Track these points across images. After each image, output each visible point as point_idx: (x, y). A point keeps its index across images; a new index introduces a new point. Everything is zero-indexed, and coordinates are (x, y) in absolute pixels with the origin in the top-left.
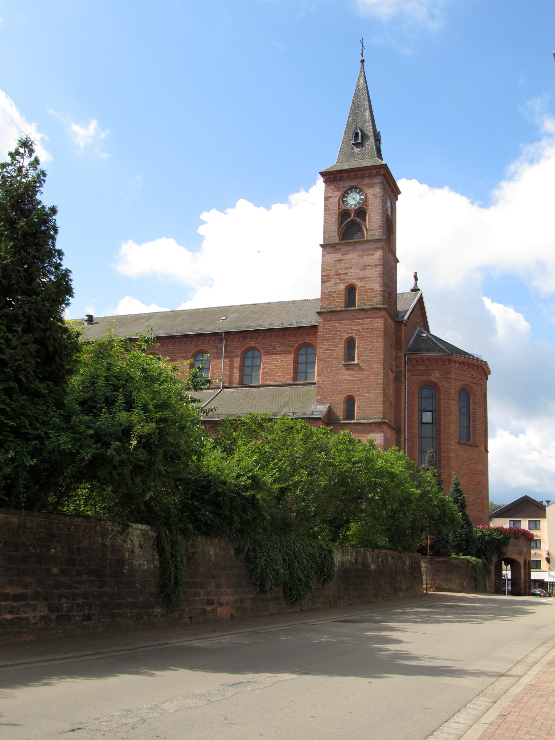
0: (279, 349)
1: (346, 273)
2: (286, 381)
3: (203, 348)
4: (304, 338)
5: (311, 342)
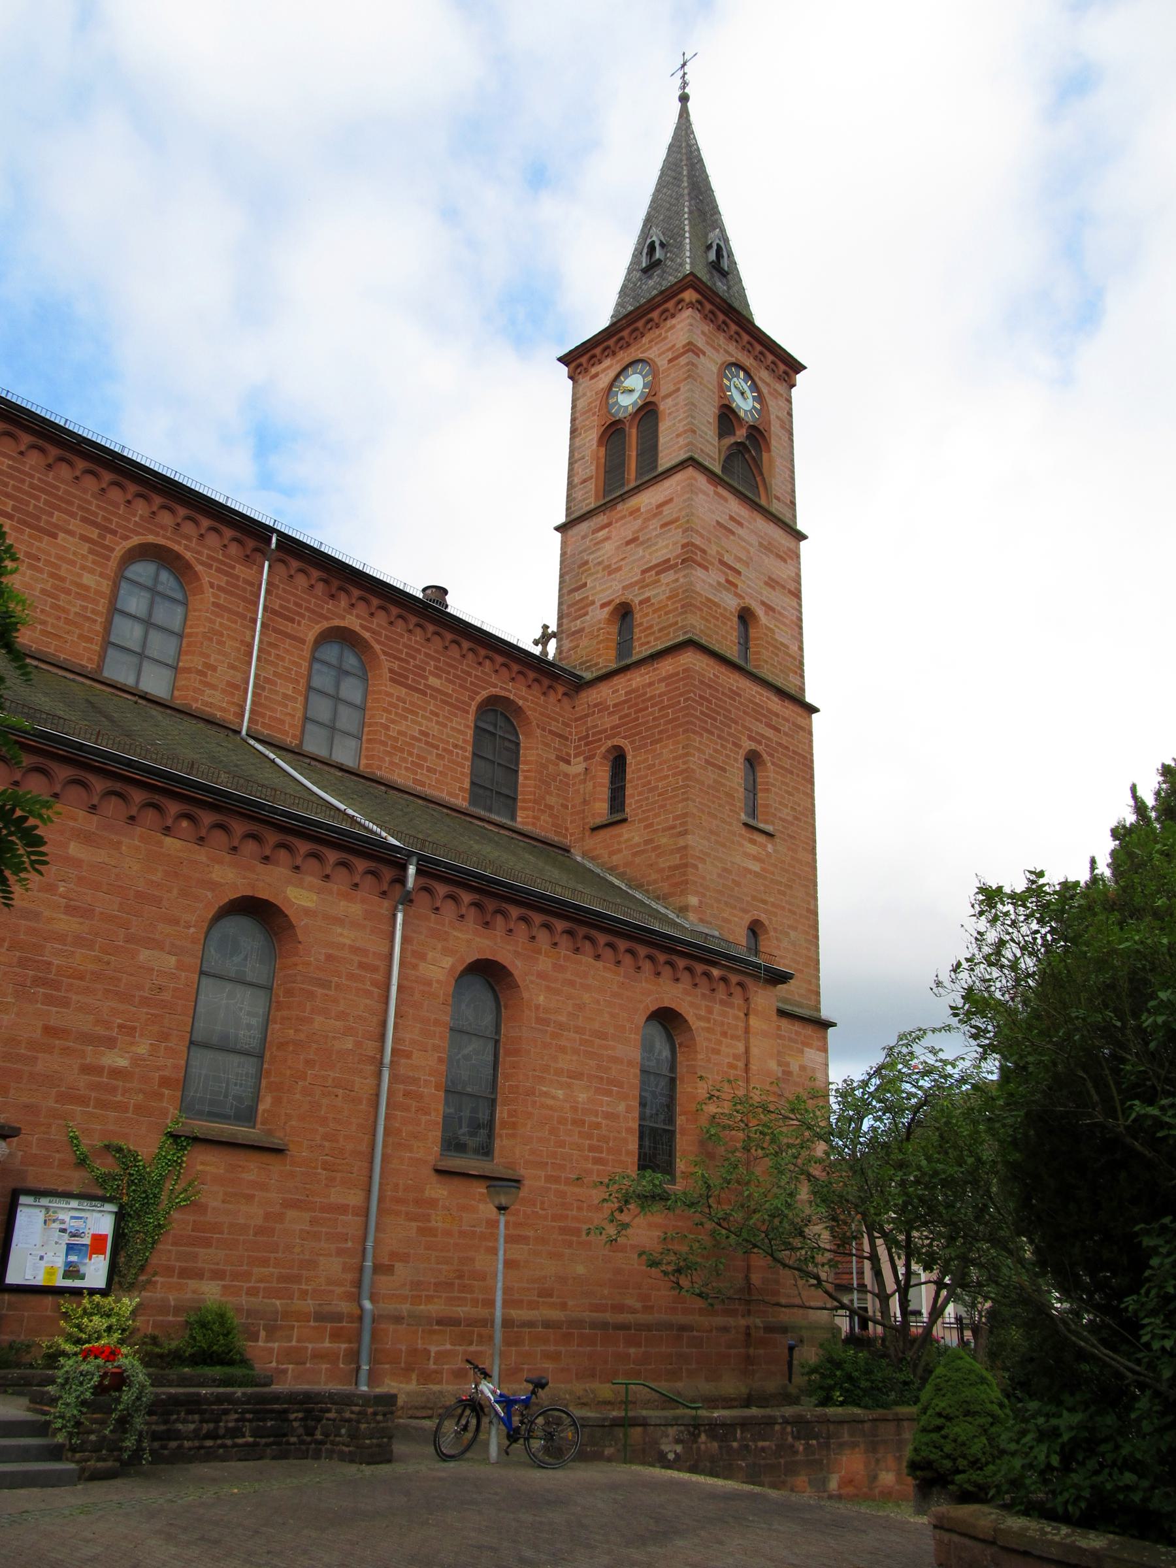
0: (433, 681)
1: (739, 573)
2: (450, 794)
3: (176, 547)
4: (504, 682)
5: (520, 703)
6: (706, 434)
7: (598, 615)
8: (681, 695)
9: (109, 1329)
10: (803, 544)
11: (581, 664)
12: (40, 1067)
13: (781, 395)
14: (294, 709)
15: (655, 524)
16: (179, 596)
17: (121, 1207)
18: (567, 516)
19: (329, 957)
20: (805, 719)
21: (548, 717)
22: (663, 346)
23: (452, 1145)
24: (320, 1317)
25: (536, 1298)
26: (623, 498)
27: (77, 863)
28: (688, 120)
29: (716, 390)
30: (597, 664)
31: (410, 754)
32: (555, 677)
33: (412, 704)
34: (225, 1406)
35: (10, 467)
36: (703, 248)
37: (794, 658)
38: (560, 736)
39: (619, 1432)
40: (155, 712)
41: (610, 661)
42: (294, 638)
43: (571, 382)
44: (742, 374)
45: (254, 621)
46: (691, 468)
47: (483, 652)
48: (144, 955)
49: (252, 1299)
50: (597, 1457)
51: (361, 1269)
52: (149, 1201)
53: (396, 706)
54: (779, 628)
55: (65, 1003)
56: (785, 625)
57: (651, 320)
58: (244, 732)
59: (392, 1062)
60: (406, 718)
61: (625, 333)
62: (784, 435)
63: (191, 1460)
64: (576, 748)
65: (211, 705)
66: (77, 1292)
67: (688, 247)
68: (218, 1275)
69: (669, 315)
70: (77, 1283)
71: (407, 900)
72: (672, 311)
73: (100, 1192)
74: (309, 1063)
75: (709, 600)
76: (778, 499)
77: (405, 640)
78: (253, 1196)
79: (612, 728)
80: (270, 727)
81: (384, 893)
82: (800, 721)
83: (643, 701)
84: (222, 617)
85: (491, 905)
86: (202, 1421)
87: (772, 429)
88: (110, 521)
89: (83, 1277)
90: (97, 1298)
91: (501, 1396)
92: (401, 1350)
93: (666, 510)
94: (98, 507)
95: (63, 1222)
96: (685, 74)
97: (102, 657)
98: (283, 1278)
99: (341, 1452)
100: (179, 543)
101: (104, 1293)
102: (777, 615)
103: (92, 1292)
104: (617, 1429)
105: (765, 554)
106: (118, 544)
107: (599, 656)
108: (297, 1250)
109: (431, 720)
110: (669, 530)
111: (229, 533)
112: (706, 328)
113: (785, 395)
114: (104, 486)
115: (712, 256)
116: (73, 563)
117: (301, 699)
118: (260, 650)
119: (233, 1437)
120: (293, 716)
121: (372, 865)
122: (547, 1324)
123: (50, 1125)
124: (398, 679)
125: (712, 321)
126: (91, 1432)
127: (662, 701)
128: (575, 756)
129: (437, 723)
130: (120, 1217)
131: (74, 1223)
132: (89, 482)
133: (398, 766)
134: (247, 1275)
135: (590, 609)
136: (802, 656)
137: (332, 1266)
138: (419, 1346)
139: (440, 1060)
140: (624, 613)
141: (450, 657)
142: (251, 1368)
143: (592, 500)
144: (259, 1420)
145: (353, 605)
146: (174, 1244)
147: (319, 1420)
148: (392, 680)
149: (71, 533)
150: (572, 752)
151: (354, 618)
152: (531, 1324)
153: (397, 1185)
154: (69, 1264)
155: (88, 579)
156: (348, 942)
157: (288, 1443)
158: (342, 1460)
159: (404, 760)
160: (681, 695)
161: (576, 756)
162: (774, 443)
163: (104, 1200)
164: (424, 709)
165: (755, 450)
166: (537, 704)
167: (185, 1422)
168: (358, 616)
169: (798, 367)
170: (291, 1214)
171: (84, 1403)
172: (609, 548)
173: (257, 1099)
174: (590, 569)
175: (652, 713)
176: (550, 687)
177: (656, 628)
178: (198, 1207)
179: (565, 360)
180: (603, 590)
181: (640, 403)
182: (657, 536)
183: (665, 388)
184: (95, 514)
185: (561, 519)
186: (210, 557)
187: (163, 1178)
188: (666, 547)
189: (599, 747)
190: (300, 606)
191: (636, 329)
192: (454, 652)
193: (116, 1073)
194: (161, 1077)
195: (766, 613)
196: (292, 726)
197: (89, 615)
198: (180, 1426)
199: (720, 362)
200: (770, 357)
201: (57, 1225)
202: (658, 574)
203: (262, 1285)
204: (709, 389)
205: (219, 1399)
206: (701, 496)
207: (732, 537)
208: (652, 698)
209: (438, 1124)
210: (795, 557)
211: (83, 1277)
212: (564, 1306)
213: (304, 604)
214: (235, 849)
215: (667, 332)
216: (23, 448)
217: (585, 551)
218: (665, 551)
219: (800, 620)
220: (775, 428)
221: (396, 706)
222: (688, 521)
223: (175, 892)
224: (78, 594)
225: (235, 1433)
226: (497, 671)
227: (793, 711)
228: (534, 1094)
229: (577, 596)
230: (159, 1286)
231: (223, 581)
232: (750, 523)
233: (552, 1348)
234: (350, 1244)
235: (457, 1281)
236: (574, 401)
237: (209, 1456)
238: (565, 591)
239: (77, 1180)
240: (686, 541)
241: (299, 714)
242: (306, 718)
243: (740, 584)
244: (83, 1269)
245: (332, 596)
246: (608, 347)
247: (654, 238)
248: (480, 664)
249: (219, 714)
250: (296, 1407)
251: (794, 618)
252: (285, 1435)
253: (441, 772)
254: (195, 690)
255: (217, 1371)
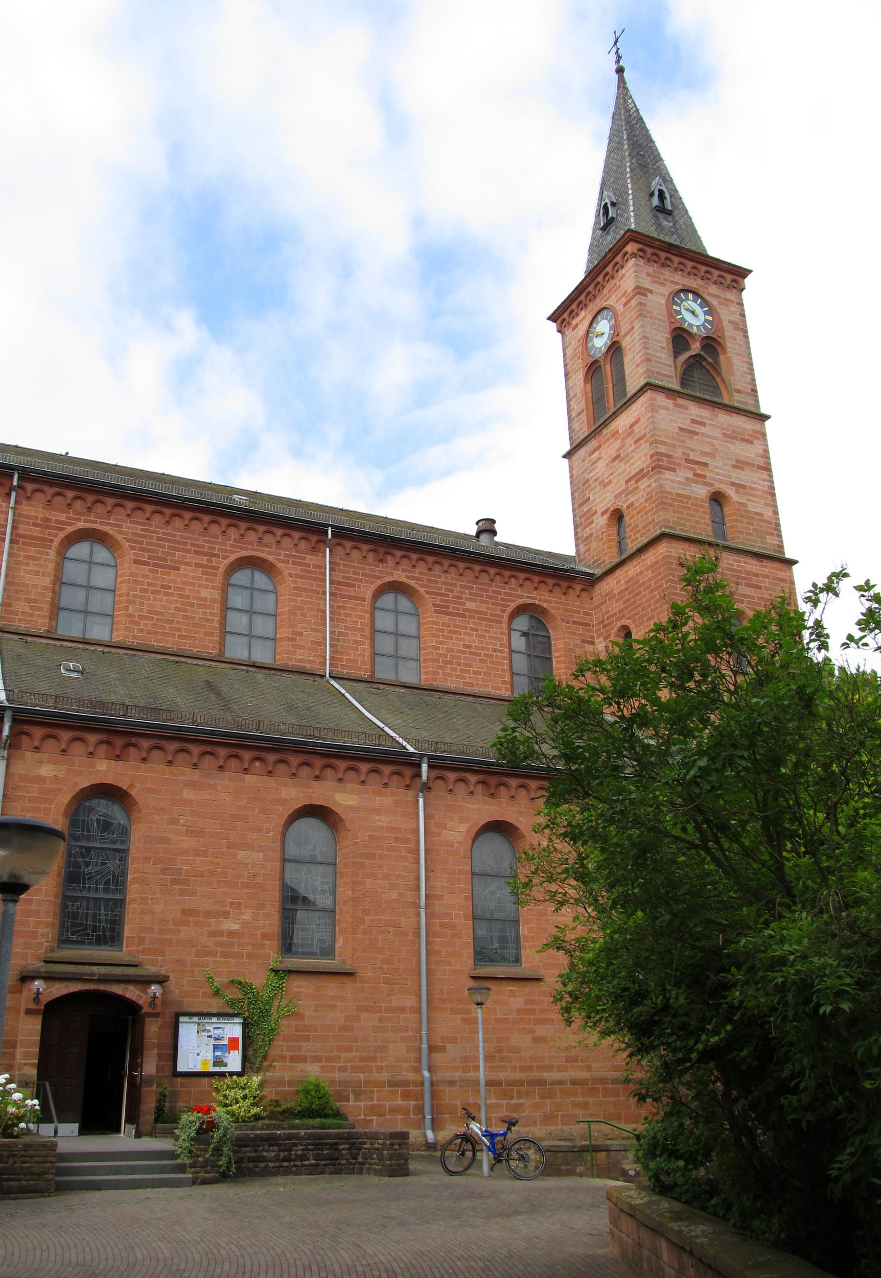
0: (470, 605)
1: (706, 465)
3: (261, 555)
5: (545, 605)
6: (661, 358)
7: (601, 521)
8: (663, 578)
9: (245, 1097)
10: (767, 423)
11: (594, 563)
12: (183, 935)
13: (732, 301)
14: (364, 650)
15: (630, 441)
16: (271, 588)
17: (245, 1019)
18: (571, 444)
19: (371, 837)
20: (785, 572)
21: (571, 611)
22: (619, 293)
23: (481, 955)
24: (393, 1084)
25: (564, 1063)
26: (605, 424)
27: (189, 802)
28: (625, 88)
29: (666, 319)
30: (604, 561)
31: (459, 664)
32: (571, 579)
33: (455, 626)
34: (294, 1141)
35: (142, 530)
36: (647, 197)
37: (771, 523)
38: (583, 624)
39: (588, 1156)
40: (260, 676)
41: (613, 557)
42: (357, 598)
43: (559, 335)
44: (690, 296)
45: (324, 593)
46: (649, 391)
47: (507, 573)
48: (241, 855)
49: (343, 1074)
50: (571, 1173)
51: (419, 1050)
52: (264, 1014)
53: (442, 631)
54: (751, 501)
55: (194, 893)
56: (757, 496)
57: (607, 274)
58: (327, 675)
59: (426, 904)
60: (452, 638)
61: (591, 288)
62: (739, 335)
63: (275, 1174)
64: (598, 630)
65: (302, 660)
66: (222, 1075)
67: (631, 203)
68: (316, 1059)
69: (618, 267)
70: (223, 1069)
71: (426, 788)
72: (621, 263)
73: (231, 1011)
74: (366, 912)
75: (678, 495)
76: (738, 391)
77: (443, 579)
78: (335, 1006)
79: (620, 612)
80: (348, 667)
81: (408, 786)
82: (781, 574)
83: (638, 587)
84: (301, 596)
85: (493, 781)
86: (279, 1151)
87: (726, 333)
88: (214, 549)
89: (226, 1065)
90: (235, 1077)
91: (486, 1131)
92: (457, 1105)
93: (636, 429)
94: (204, 541)
95: (209, 1031)
96: (618, 49)
97: (222, 643)
98: (362, 1059)
99: (375, 1170)
100: (263, 551)
101: (240, 1074)
102: (749, 491)
103: (232, 1074)
104: (585, 1154)
105: (731, 442)
106: (221, 563)
107: (605, 554)
108: (371, 1039)
109: (472, 636)
110: (640, 445)
111: (297, 535)
112: (650, 269)
113: (736, 300)
114: (206, 526)
115: (655, 201)
116: (193, 584)
117: (367, 641)
118: (331, 613)
119: (302, 1160)
120: (363, 655)
121: (395, 768)
122: (574, 1082)
123: (193, 972)
124: (441, 609)
125: (656, 262)
126: (198, 1156)
127: (650, 585)
128: (598, 638)
129: (477, 636)
130: (245, 1025)
131: (216, 1031)
132: (196, 526)
133: (451, 675)
134: (338, 1058)
135: (594, 517)
136: (778, 519)
137: (398, 1049)
138: (471, 1101)
139: (466, 898)
140: (618, 516)
141: (481, 584)
142: (347, 1119)
143: (586, 428)
144: (318, 1149)
145: (398, 563)
146: (284, 1041)
147: (360, 1149)
148: (436, 611)
149: (187, 564)
150: (595, 635)
151: (400, 573)
152: (561, 1082)
153: (442, 990)
154: (215, 1057)
155: (204, 593)
156: (385, 825)
157: (340, 1164)
158: (375, 1174)
159: (455, 670)
160: (663, 578)
161: (598, 637)
162: (729, 345)
163: (237, 1015)
164: (465, 628)
165: (711, 357)
166: (559, 603)
167: (268, 1151)
168: (403, 571)
169: (743, 273)
170: (364, 1015)
171: (192, 1139)
172: (601, 465)
173: (334, 940)
174: (590, 485)
175: (645, 596)
176: (569, 587)
177: (640, 526)
178: (296, 1015)
179: (553, 318)
180: (601, 502)
181: (609, 343)
182: (633, 451)
183: (623, 330)
184: (202, 547)
185: (567, 448)
186: (286, 555)
187: (272, 999)
188: (640, 460)
189: (612, 628)
190: (358, 574)
191: (598, 283)
192: (484, 578)
193: (232, 934)
194: (262, 934)
195: (737, 492)
196: (363, 663)
197: (208, 617)
198: (265, 1154)
199: (667, 293)
200: (716, 273)
201: (206, 1034)
202: (637, 482)
203: (349, 1064)
204: (659, 320)
205: (289, 1137)
206: (662, 411)
207: (695, 437)
208: (644, 583)
209: (469, 943)
210: (761, 437)
211: (226, 1065)
212: (589, 1068)
213: (361, 572)
214: (294, 774)
215: (620, 281)
216: (148, 515)
217: (585, 471)
218: (639, 463)
219: (773, 488)
220: (729, 331)
221: (442, 631)
222: (652, 436)
223: (257, 810)
224: (199, 604)
225: (302, 1158)
226: (521, 585)
227: (772, 568)
228: (546, 914)
229: (585, 508)
230: (277, 1068)
231: (298, 570)
232: (712, 420)
233: (581, 1099)
234: (410, 1033)
235: (497, 1055)
236: (564, 350)
237: (286, 1172)
238: (576, 505)
239: (215, 1005)
240: (652, 452)
241: (368, 653)
242: (375, 654)
243: (708, 474)
244: (225, 1060)
245: (381, 561)
246: (581, 302)
247: (607, 201)
248: (506, 583)
249: (308, 666)
250: (343, 1141)
251: (766, 489)
252: (337, 1159)
253: (485, 673)
254: (289, 652)
255: (318, 1121)
